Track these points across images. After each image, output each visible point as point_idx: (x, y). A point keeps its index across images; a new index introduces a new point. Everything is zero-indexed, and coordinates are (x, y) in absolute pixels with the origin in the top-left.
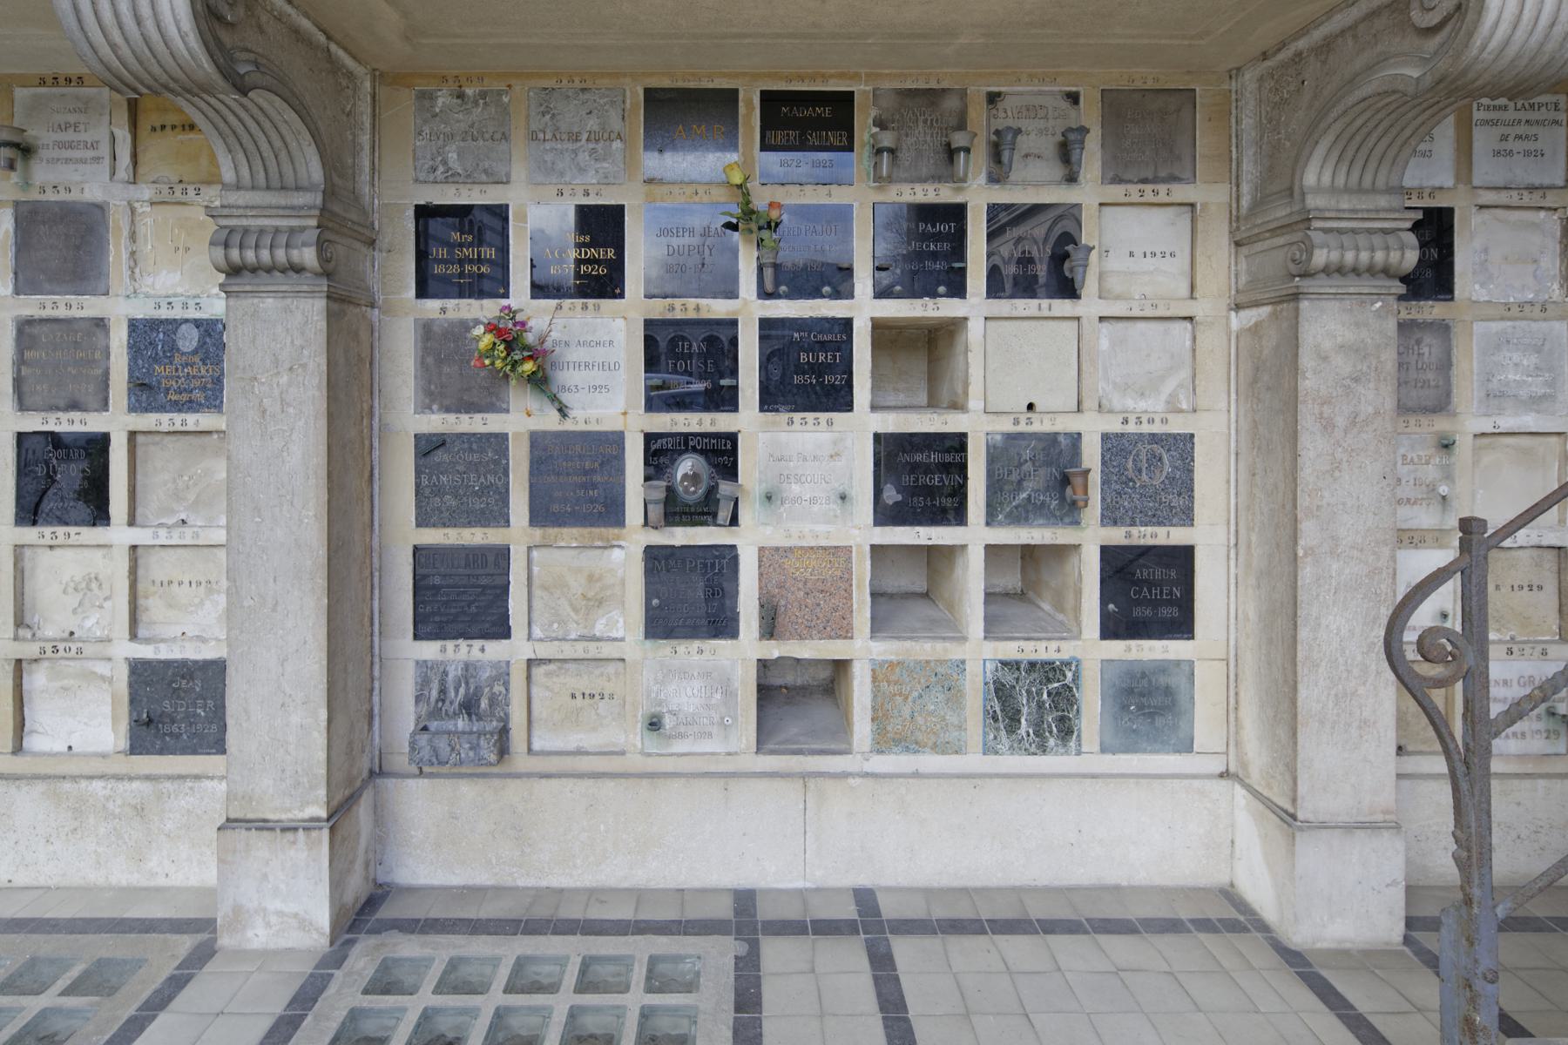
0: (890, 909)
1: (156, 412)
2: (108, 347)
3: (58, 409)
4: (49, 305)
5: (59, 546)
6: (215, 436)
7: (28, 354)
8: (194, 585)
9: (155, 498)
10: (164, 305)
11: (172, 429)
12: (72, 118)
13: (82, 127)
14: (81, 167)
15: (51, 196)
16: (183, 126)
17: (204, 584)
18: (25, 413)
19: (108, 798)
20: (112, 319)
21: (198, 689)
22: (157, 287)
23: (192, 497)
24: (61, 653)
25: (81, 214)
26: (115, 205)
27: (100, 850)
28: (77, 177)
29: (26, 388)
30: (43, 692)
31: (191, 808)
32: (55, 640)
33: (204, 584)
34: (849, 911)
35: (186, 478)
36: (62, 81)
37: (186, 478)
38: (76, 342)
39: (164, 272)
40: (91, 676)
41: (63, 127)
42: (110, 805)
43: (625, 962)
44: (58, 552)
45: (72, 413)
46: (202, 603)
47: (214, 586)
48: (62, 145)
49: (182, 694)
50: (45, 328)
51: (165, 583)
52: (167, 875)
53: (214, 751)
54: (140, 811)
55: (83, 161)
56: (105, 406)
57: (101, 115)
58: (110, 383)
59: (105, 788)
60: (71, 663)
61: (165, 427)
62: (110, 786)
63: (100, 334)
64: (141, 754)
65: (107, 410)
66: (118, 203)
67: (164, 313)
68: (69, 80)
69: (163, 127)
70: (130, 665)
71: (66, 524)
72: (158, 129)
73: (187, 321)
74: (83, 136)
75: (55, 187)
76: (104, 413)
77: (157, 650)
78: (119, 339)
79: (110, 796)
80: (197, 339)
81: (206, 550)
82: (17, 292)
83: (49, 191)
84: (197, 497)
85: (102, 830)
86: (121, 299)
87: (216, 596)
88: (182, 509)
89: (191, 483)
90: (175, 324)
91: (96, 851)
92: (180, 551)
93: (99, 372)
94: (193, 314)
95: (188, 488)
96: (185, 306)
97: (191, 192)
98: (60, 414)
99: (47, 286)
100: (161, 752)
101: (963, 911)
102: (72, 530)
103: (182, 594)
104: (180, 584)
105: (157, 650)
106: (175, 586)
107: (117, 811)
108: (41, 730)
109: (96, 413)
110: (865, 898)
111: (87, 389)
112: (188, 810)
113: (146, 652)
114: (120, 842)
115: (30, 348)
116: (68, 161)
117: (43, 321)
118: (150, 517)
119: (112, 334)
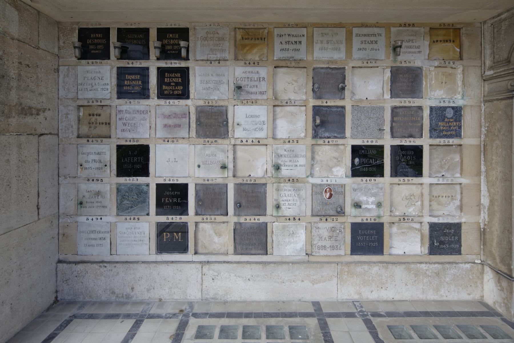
0: (326, 310)
1: (439, 138)
2: (423, 116)
3: (405, 137)
4: (403, 102)
5: (401, 184)
6: (454, 146)
7: (395, 119)
8: (447, 197)
9: (434, 168)
10: (442, 102)
11: (444, 144)
12: (411, 38)
13: (414, 41)
14: (414, 55)
15: (404, 65)
16: (444, 41)
17: (450, 197)
18: (394, 138)
19: (427, 270)
20: (424, 107)
21: (452, 233)
22: (435, 95)
23: (447, 167)
24: (406, 220)
25: (414, 70)
26: (426, 68)
27: (424, 288)
28: (413, 58)
29: (394, 130)
30: (395, 234)
31: (455, 273)
32: (400, 216)
33: (450, 197)
34: (311, 310)
35: (444, 161)
36: (407, 25)
37: (444, 161)
38: (412, 114)
39: (438, 90)
40: (412, 228)
41: (408, 41)
42: (428, 272)
43: (235, 328)
44: (401, 186)
45: (410, 139)
46: (450, 203)
47: (454, 198)
48: (408, 47)
49: (447, 234)
50: (401, 110)
51: (437, 197)
52: (447, 296)
53: (458, 254)
54: (438, 274)
55: (415, 53)
56: (421, 136)
57: (421, 37)
58: (423, 128)
59: (426, 267)
60: (405, 224)
61: (442, 144)
62: (427, 266)
63: (420, 111)
64: (433, 255)
65: (422, 138)
66: (427, 67)
67: (442, 105)
68: (409, 25)
69: (437, 41)
70: (429, 225)
71: (407, 176)
72: (436, 42)
73: (449, 107)
74: (415, 44)
75: (405, 61)
76: (421, 139)
77: (439, 219)
78: (426, 113)
79: (428, 269)
80: (453, 113)
81: (451, 185)
82: (391, 98)
83: (403, 63)
84: (449, 167)
85: (425, 281)
86: (427, 100)
87: (454, 201)
88: (443, 171)
89: (446, 162)
90: (445, 108)
91: (422, 288)
92: (442, 186)
93: (420, 124)
94: (452, 105)
95: (445, 164)
96: (449, 102)
97: (447, 63)
98: (406, 139)
99: (402, 96)
100: (440, 254)
101: (412, 309)
102: (410, 178)
103: (443, 200)
104: (442, 197)
105: (439, 219)
106: (441, 198)
107: (430, 274)
108: (394, 247)
109: (418, 139)
110: (316, 304)
111: (415, 130)
112: (454, 274)
113: (435, 220)
114: (431, 285)
115: (396, 116)
116: (410, 52)
117: (400, 107)
118: (433, 174)
119: (424, 112)
